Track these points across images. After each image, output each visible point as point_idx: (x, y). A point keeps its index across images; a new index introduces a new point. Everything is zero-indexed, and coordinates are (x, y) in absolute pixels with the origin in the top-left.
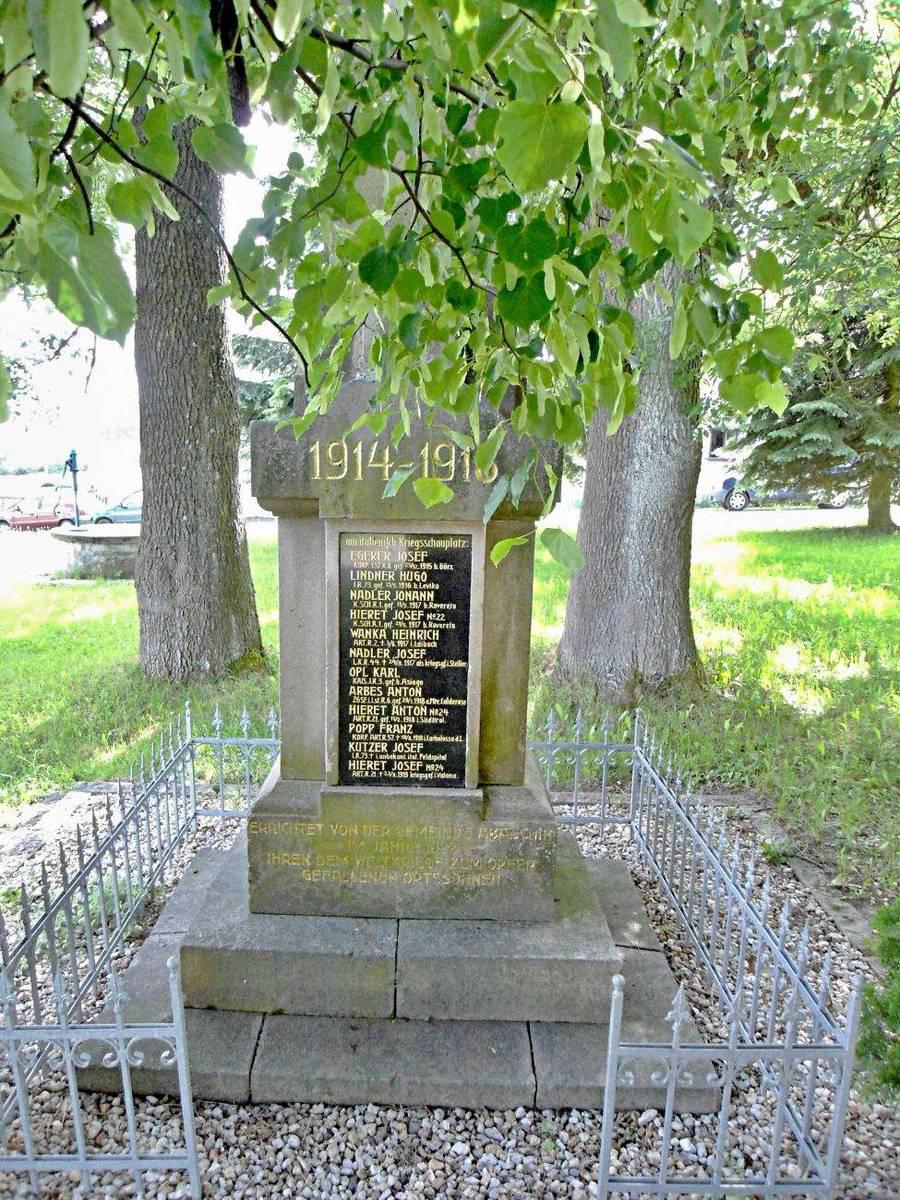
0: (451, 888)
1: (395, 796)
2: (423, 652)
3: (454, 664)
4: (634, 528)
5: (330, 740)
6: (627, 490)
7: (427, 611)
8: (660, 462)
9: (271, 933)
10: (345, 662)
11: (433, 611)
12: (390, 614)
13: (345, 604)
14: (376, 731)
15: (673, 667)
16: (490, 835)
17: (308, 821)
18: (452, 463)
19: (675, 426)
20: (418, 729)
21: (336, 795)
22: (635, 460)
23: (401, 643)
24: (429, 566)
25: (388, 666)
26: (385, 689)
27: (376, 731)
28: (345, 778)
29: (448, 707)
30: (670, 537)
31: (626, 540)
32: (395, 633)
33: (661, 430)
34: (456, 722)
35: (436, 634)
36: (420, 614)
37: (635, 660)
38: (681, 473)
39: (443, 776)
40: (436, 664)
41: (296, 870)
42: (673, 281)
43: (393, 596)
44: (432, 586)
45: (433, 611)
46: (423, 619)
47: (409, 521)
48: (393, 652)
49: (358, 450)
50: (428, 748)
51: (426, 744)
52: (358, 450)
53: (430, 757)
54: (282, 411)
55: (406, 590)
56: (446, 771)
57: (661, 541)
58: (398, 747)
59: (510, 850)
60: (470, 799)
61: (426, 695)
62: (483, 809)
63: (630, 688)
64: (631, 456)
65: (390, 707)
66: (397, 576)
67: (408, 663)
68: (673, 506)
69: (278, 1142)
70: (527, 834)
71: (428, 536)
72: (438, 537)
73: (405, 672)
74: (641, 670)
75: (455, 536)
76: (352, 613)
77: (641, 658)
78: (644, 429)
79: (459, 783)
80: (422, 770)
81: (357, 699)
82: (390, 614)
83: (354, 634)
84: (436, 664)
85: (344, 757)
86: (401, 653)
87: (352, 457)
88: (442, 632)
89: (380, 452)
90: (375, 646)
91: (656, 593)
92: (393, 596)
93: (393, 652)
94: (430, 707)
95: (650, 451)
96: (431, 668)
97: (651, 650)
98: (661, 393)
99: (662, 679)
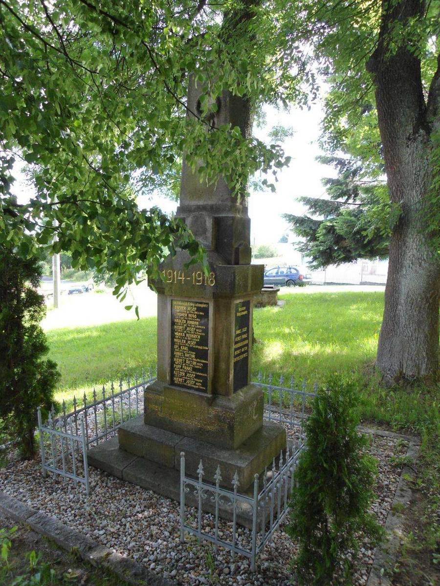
0: (201, 429)
1: (184, 392)
2: (195, 343)
3: (204, 348)
4: (403, 301)
5: (168, 369)
6: (400, 283)
7: (196, 328)
8: (416, 271)
9: (156, 434)
10: (173, 343)
11: (199, 329)
12: (186, 328)
13: (173, 323)
14: (182, 368)
15: (423, 373)
16: (213, 412)
17: (160, 395)
18: (201, 278)
19: (426, 253)
20: (194, 369)
21: (168, 388)
22: (404, 269)
23: (189, 339)
24: (197, 313)
25: (185, 346)
26: (184, 354)
27: (182, 368)
28: (172, 383)
29: (203, 363)
30: (423, 307)
31: (400, 307)
32: (187, 335)
33: (417, 255)
34: (204, 369)
35: (199, 337)
36: (194, 329)
37: (401, 366)
38: (429, 276)
39: (201, 388)
40: (199, 347)
41: (156, 412)
42: (425, 183)
43: (186, 322)
44: (198, 320)
45: (199, 329)
46: (195, 331)
47: (190, 297)
48: (187, 342)
49: (175, 273)
50: (197, 377)
51: (196, 375)
52: (175, 273)
53: (197, 380)
54: (324, 235)
55: (190, 320)
56: (202, 386)
57: (417, 309)
58: (188, 374)
59: (218, 418)
60: (207, 397)
61: (196, 358)
62: (211, 402)
63: (397, 380)
64: (402, 267)
65: (185, 360)
66: (188, 315)
67: (191, 346)
68: (424, 292)
69: (119, 490)
70: (224, 414)
71: (196, 303)
72: (201, 303)
73: (191, 349)
74: (404, 371)
75: (205, 303)
76: (175, 327)
77: (405, 366)
78: (409, 254)
79: (205, 391)
80: (195, 384)
81: (176, 356)
82: (186, 328)
83: (176, 334)
84: (199, 347)
85: (172, 376)
86: (189, 342)
87: (174, 276)
88: (201, 336)
89: (181, 273)
90: (181, 338)
91: (414, 334)
92: (186, 322)
93: (187, 342)
94: (197, 362)
95: (411, 265)
96: (197, 348)
97: (410, 362)
98: (418, 237)
99: (415, 378)
